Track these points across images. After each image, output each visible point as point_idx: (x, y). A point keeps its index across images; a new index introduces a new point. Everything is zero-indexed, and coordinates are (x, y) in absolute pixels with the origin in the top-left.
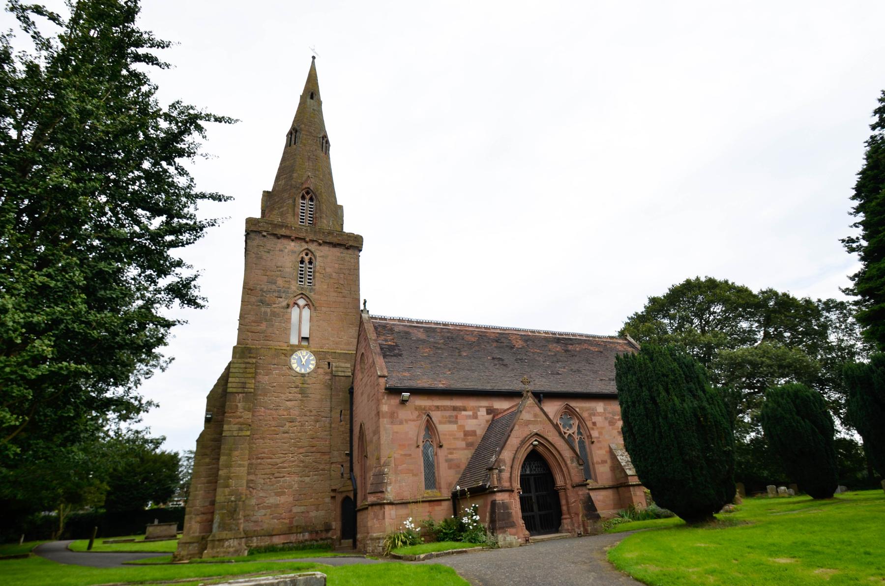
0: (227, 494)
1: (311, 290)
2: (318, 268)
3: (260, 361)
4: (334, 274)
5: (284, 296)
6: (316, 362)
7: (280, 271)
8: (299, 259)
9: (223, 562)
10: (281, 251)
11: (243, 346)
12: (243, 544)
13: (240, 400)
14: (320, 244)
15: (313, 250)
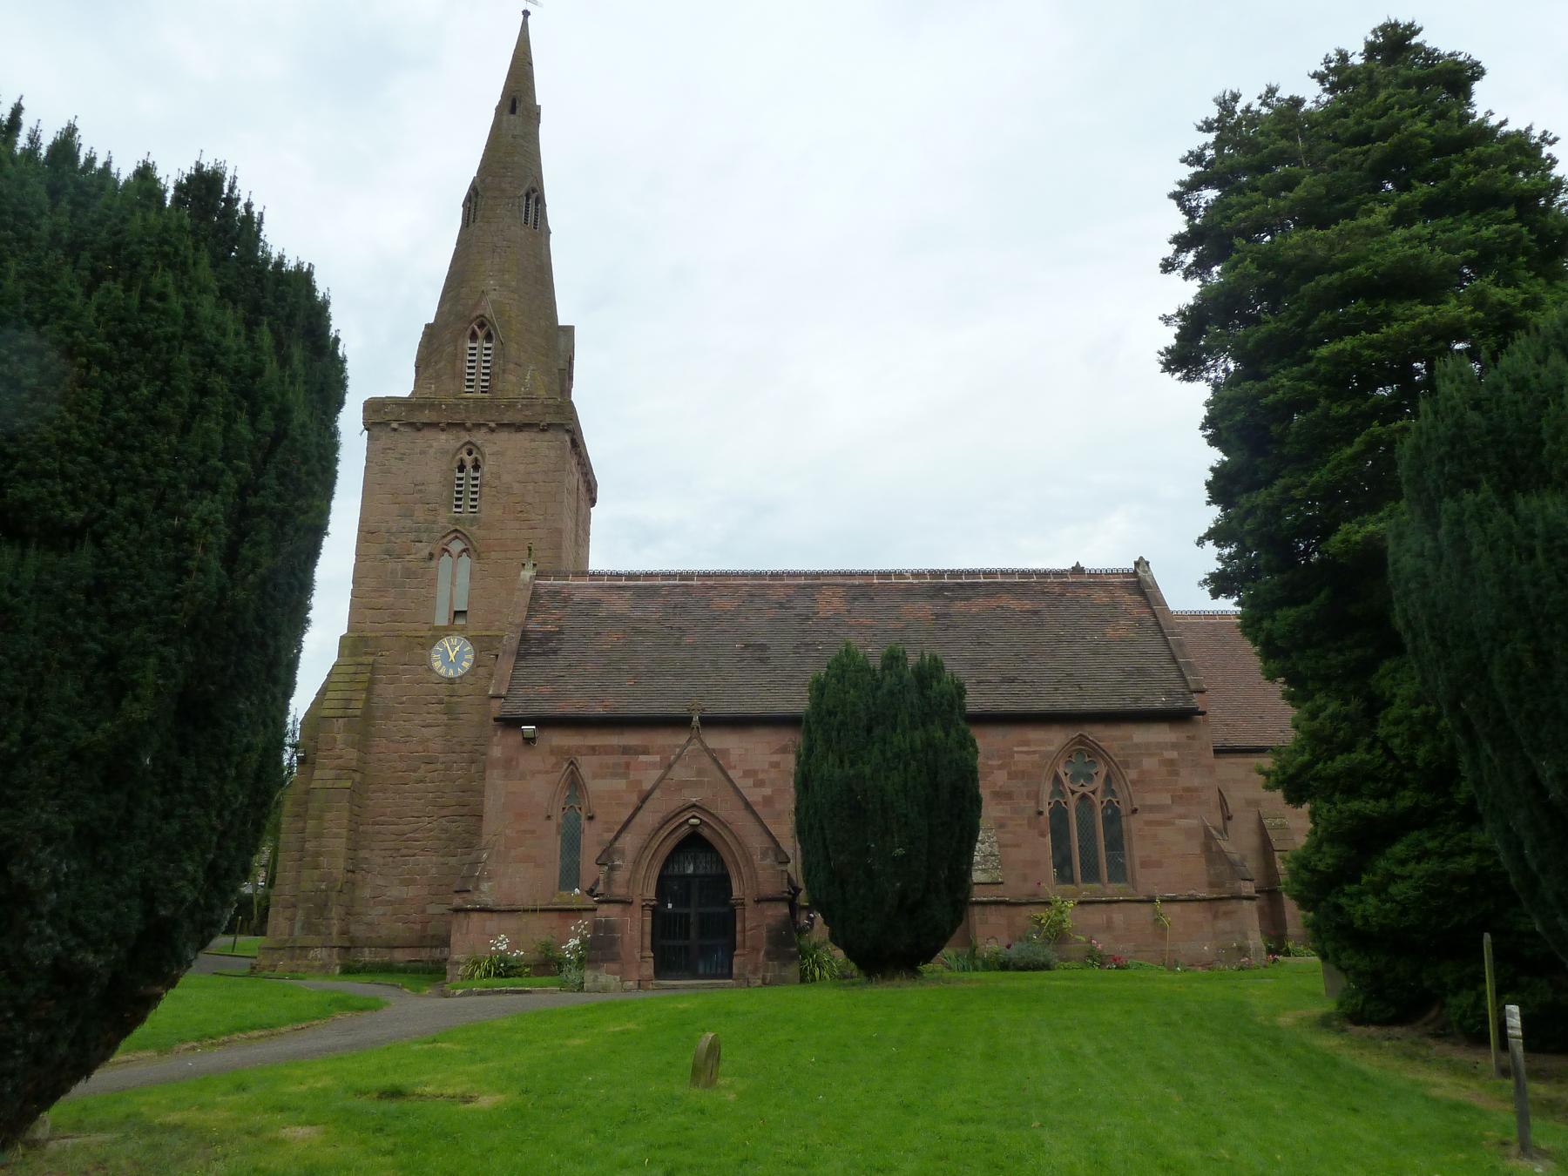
0: (315, 878)
1: (474, 521)
2: (488, 477)
3: (381, 660)
4: (516, 486)
5: (425, 539)
6: (475, 657)
7: (420, 491)
8: (456, 464)
9: (379, 984)
10: (423, 453)
11: (356, 635)
12: (335, 957)
13: (339, 729)
14: (492, 430)
15: (479, 443)
